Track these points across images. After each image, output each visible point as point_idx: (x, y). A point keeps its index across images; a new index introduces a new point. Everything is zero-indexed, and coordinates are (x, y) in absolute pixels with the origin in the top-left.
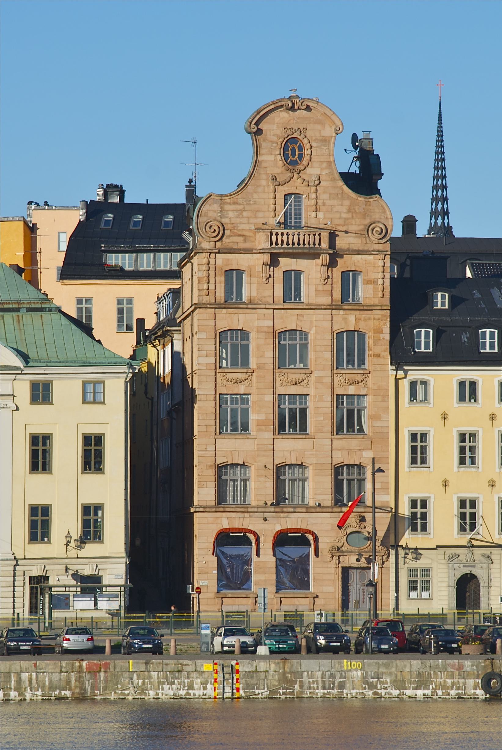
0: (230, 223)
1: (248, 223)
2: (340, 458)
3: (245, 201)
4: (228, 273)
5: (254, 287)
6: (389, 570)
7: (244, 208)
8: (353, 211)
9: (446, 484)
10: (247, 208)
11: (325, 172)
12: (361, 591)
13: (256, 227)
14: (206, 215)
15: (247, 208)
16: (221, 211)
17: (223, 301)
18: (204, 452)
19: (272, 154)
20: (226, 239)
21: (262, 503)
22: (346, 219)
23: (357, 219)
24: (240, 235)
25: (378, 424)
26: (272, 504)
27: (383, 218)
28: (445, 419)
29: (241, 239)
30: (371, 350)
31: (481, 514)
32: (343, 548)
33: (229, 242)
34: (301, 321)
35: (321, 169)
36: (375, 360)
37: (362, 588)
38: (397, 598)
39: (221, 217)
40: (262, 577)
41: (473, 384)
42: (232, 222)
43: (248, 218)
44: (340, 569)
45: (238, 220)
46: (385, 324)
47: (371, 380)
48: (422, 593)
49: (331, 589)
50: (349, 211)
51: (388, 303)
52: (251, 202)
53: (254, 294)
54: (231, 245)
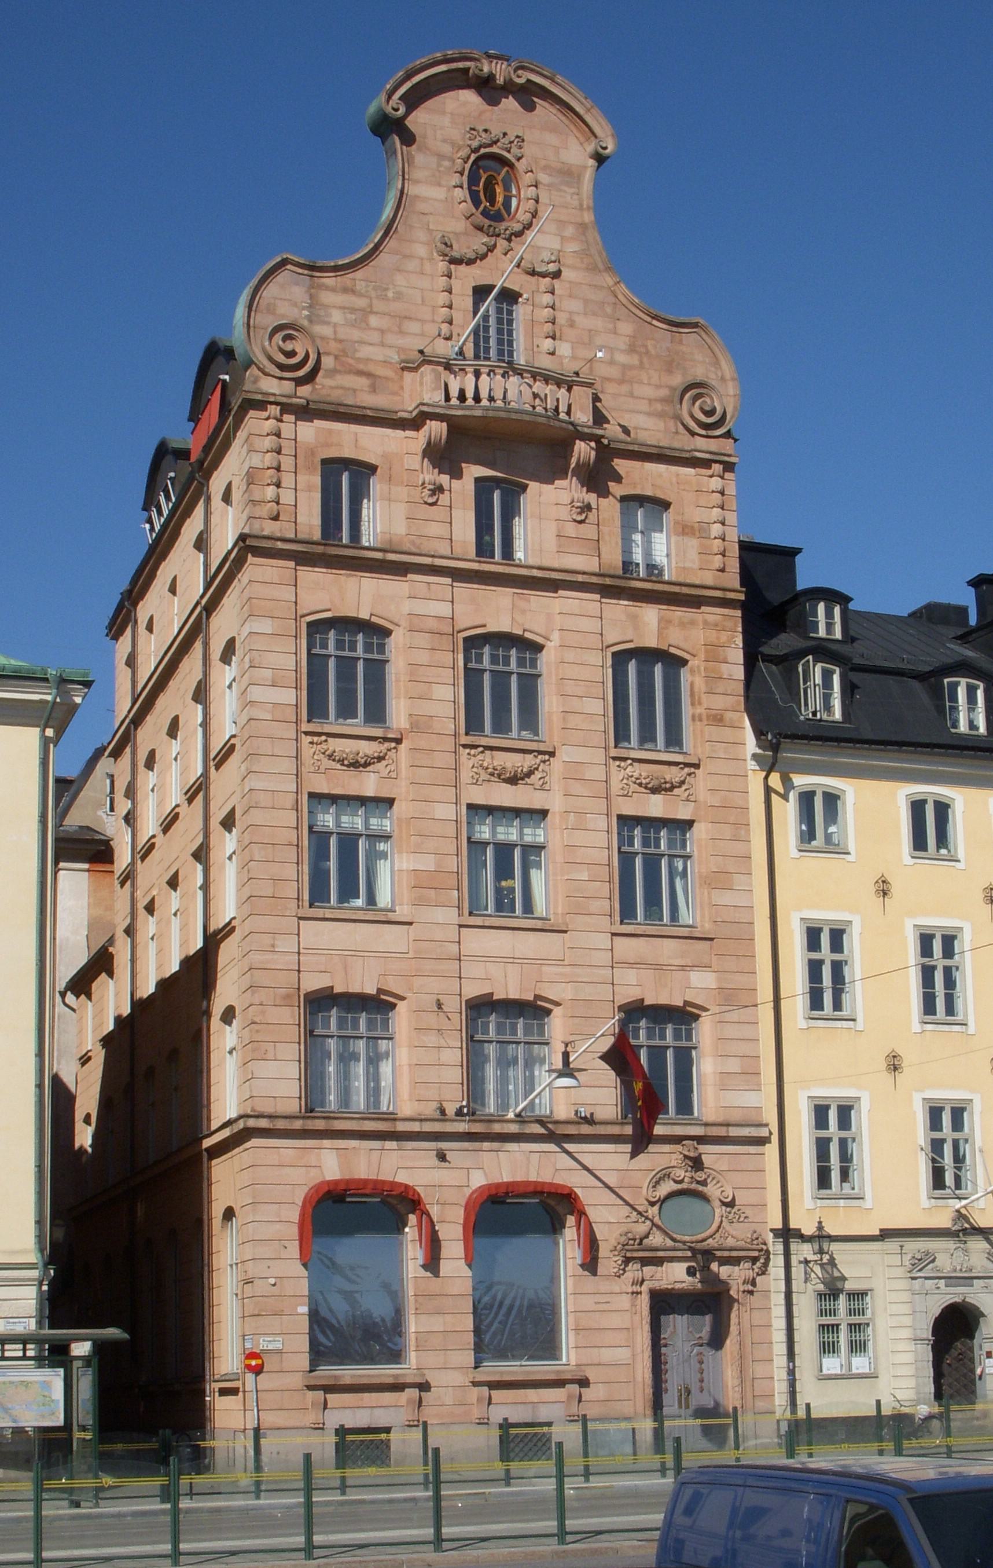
0: (335, 340)
1: (383, 344)
2: (637, 986)
3: (375, 289)
4: (333, 468)
5: (400, 510)
6: (768, 1298)
7: (371, 306)
8: (643, 350)
9: (894, 1065)
10: (379, 306)
11: (572, 247)
12: (694, 1361)
13: (403, 357)
14: (271, 310)
15: (379, 306)
16: (311, 307)
17: (317, 535)
18: (269, 956)
19: (439, 185)
20: (324, 377)
21: (430, 1109)
22: (625, 367)
23: (652, 372)
24: (360, 373)
25: (726, 898)
26: (459, 1113)
27: (713, 376)
28: (885, 894)
29: (363, 382)
30: (700, 703)
31: (978, 1143)
32: (651, 1237)
33: (332, 388)
34: (523, 612)
35: (562, 238)
36: (714, 732)
37: (696, 1350)
38: (791, 1372)
39: (311, 321)
40: (437, 1324)
41: (942, 809)
42: (341, 336)
43: (382, 332)
44: (644, 1301)
45: (356, 334)
46: (731, 640)
47: (701, 783)
48: (824, 1360)
49: (622, 1354)
50: (632, 349)
51: (736, 584)
52: (390, 294)
53: (400, 529)
54: (336, 396)
